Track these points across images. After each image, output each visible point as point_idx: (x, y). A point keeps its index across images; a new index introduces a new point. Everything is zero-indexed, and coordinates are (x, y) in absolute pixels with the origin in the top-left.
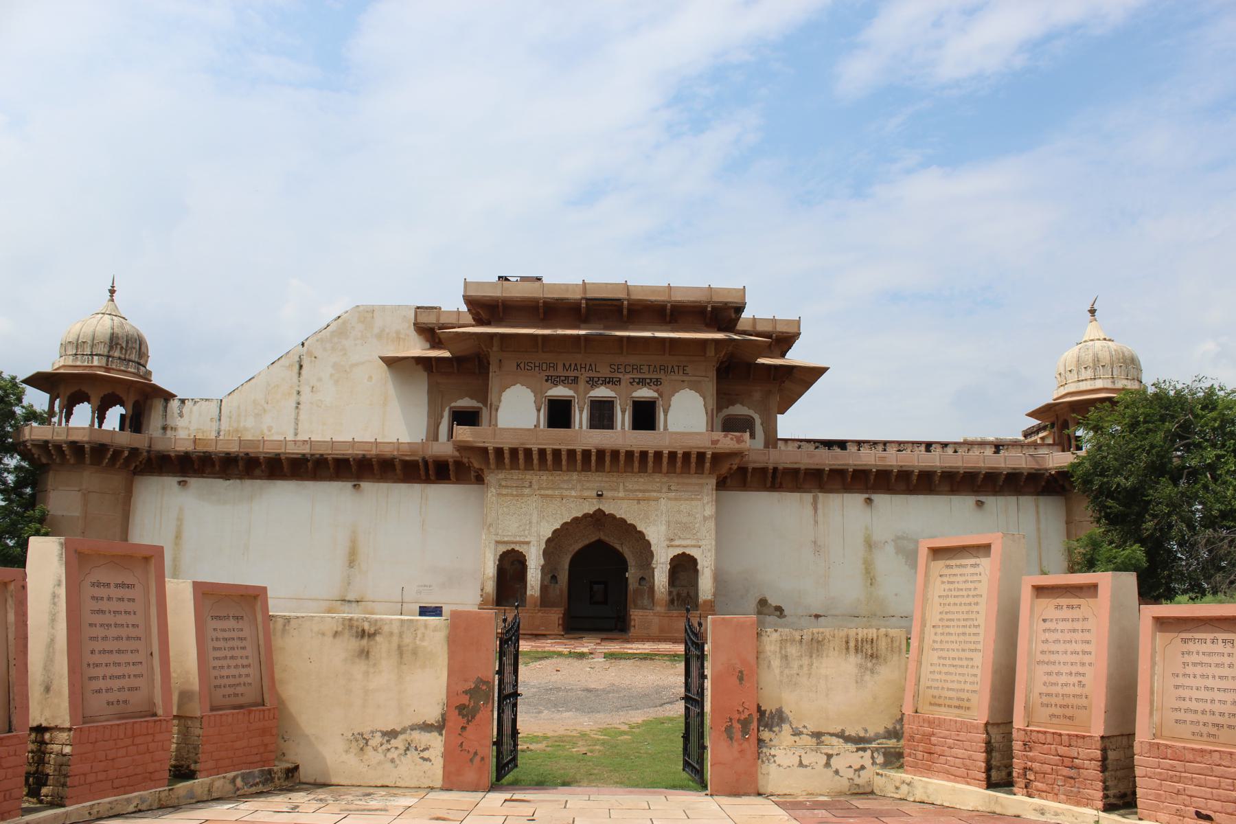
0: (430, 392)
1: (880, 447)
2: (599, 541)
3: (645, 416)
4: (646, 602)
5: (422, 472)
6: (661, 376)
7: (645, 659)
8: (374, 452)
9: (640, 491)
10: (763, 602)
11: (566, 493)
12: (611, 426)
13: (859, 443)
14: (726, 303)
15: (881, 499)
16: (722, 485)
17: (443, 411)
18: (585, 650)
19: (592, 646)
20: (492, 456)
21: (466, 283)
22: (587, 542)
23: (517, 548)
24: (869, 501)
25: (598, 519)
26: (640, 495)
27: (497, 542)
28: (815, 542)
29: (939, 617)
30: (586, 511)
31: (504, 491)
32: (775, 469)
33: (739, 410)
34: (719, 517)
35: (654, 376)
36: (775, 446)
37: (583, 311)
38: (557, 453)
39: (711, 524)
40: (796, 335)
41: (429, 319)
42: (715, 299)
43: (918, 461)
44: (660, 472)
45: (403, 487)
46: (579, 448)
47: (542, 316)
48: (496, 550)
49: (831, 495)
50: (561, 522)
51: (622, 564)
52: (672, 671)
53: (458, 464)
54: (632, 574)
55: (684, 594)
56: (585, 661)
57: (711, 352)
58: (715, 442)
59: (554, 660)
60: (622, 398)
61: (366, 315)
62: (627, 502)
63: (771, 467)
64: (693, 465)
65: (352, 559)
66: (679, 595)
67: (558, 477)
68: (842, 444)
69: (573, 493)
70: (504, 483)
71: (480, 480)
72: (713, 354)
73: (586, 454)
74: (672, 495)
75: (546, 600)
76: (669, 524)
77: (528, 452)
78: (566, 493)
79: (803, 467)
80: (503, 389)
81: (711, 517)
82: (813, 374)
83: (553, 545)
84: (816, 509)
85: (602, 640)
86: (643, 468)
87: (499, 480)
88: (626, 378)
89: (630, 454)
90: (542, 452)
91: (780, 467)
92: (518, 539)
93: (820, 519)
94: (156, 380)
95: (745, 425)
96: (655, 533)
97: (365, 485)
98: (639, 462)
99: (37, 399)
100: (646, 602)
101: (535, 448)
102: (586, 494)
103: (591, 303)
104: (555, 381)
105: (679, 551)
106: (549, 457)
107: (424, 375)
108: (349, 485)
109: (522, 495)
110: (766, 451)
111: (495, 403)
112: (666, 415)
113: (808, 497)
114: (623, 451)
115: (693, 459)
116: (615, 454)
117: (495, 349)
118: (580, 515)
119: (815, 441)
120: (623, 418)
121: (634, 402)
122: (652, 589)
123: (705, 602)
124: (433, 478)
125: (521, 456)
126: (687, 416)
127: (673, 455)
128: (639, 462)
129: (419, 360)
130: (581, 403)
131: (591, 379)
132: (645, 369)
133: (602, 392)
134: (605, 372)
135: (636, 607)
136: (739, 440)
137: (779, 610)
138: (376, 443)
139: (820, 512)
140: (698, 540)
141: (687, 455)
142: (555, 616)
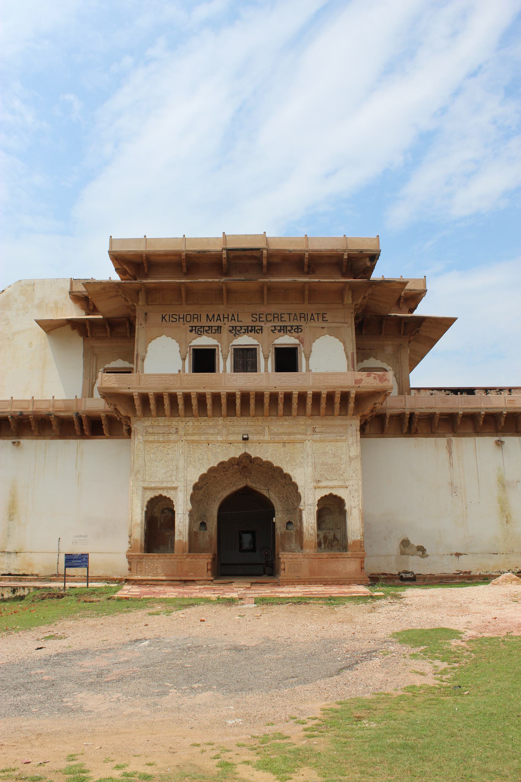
0: (85, 355)
1: (507, 392)
3: (286, 360)
4: (293, 546)
5: (77, 427)
6: (302, 323)
7: (299, 603)
8: (31, 409)
9: (285, 434)
10: (405, 543)
11: (211, 438)
13: (486, 390)
14: (361, 251)
16: (363, 431)
18: (235, 595)
19: (242, 591)
20: (137, 403)
22: (234, 489)
23: (165, 494)
24: (499, 444)
25: (245, 464)
26: (285, 438)
27: (145, 489)
28: (451, 484)
30: (232, 455)
31: (151, 438)
32: (412, 415)
33: (371, 362)
34: (364, 457)
35: (295, 323)
36: (409, 394)
37: (224, 261)
39: (357, 465)
40: (424, 292)
42: (351, 247)
44: (305, 415)
45: (60, 443)
46: (223, 391)
47: (185, 270)
48: (143, 496)
49: (464, 439)
50: (208, 467)
52: (333, 617)
53: (111, 419)
55: (331, 537)
56: (234, 608)
59: (200, 608)
60: (265, 345)
61: (27, 288)
63: (408, 412)
64: (337, 406)
65: (12, 512)
66: (325, 538)
67: (204, 423)
68: (470, 391)
69: (219, 438)
70: (150, 430)
72: (350, 301)
74: (317, 437)
75: (194, 546)
77: (173, 397)
78: (211, 438)
79: (438, 411)
81: (356, 457)
82: (443, 325)
83: (201, 490)
84: (450, 453)
85: (252, 584)
88: (267, 326)
89: (274, 397)
90: (187, 397)
91: (417, 412)
92: (165, 485)
96: (302, 475)
97: (24, 442)
100: (293, 546)
101: (179, 392)
102: (232, 438)
103: (232, 254)
104: (199, 331)
105: (326, 492)
106: (194, 402)
107: (80, 340)
108: (9, 442)
109: (169, 442)
110: (402, 397)
111: (141, 353)
113: (442, 441)
115: (337, 400)
116: (259, 396)
117: (140, 303)
118: (226, 459)
119: (445, 389)
120: (266, 363)
122: (300, 533)
123: (354, 542)
124: (87, 433)
125: (166, 401)
126: (329, 358)
127: (317, 396)
129: (73, 324)
130: (225, 351)
131: (234, 328)
132: (286, 317)
133: (245, 340)
134: (247, 321)
135: (284, 550)
136: (382, 379)
137: (421, 549)
138: (33, 401)
139: (454, 454)
140: (345, 481)
141: (331, 396)
142: (204, 561)
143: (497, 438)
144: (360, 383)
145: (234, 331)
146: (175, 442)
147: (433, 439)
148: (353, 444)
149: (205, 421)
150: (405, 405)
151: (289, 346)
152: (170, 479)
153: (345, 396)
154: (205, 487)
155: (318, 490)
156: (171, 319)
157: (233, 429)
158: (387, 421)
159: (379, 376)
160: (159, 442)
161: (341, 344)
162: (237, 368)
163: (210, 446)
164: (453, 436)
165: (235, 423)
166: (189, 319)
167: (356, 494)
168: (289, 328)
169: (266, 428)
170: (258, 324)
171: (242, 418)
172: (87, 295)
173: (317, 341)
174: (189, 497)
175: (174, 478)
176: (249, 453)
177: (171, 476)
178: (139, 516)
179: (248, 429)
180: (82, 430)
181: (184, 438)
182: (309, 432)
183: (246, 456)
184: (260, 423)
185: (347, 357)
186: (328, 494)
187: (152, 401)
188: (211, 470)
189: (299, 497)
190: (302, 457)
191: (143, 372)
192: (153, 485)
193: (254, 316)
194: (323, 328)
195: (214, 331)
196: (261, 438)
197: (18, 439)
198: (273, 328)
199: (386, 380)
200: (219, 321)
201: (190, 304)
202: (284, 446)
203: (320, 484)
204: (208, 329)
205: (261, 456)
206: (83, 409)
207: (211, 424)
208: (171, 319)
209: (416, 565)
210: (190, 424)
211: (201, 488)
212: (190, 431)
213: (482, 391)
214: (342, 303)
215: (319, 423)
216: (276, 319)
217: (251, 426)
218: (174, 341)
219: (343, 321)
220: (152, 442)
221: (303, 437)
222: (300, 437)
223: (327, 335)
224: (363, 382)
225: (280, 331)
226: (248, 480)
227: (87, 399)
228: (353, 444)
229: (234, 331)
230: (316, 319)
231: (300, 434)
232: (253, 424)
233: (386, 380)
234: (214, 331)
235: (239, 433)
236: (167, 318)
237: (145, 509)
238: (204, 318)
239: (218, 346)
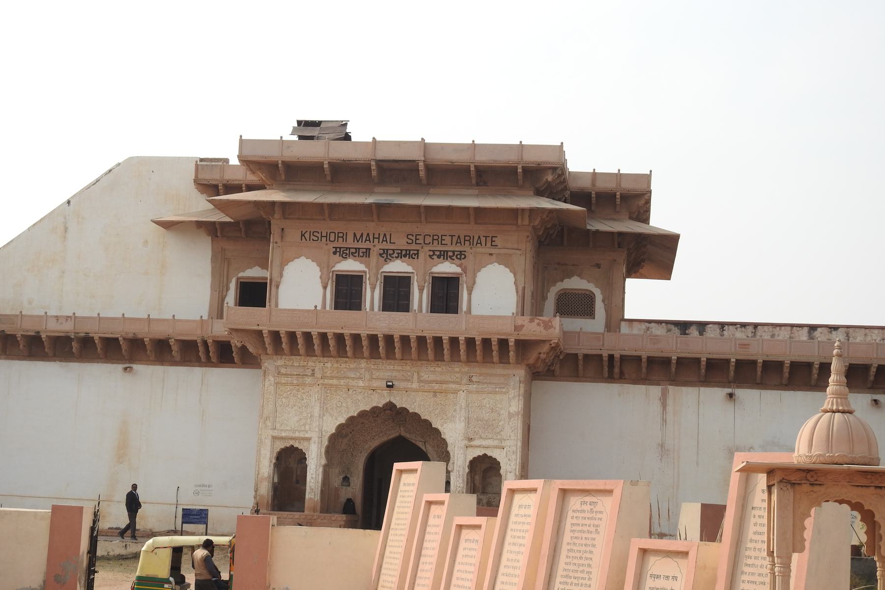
3: (446, 295)
6: (466, 248)
9: (437, 382)
11: (352, 383)
13: (722, 325)
15: (747, 395)
17: (228, 282)
21: (242, 142)
22: (385, 439)
26: (436, 386)
30: (375, 404)
31: (284, 380)
35: (458, 248)
38: (340, 338)
41: (213, 176)
49: (685, 390)
58: (518, 328)
62: (419, 392)
63: (605, 354)
69: (361, 383)
70: (283, 371)
72: (526, 222)
76: (468, 420)
77: (308, 336)
78: (352, 383)
84: (664, 405)
86: (439, 356)
87: (277, 367)
92: (297, 434)
93: (670, 417)
95: (576, 305)
102: (375, 384)
104: (344, 253)
105: (479, 452)
107: (209, 239)
108: (120, 367)
112: (470, 294)
113: (655, 391)
114: (413, 336)
117: (276, 216)
118: (368, 408)
120: (420, 297)
121: (433, 277)
126: (495, 293)
130: (373, 279)
131: (385, 251)
132: (447, 240)
133: (398, 267)
134: (401, 243)
139: (670, 408)
140: (501, 440)
143: (729, 390)
144: (520, 330)
145: (385, 255)
146: (311, 385)
147: (644, 387)
148: (514, 397)
149: (346, 362)
150: (603, 344)
151: (450, 276)
152: (303, 428)
153: (503, 343)
154: (350, 435)
155: (470, 450)
156: (312, 237)
157: (378, 374)
158: (581, 363)
159: (544, 322)
160: (292, 384)
161: (512, 275)
163: (350, 392)
164: (671, 385)
165: (380, 367)
166: (332, 239)
167: (514, 457)
168: (450, 254)
169: (415, 374)
170: (414, 247)
171: (389, 361)
173: (484, 270)
174: (323, 450)
175: (307, 427)
176: (394, 402)
177: (304, 425)
178: (266, 468)
179: (394, 374)
180: (208, 358)
181: (321, 381)
182: (464, 381)
183: (390, 406)
184: (408, 368)
185: (517, 292)
186: (481, 454)
187: (284, 340)
188: (351, 419)
190: (455, 410)
191: (277, 305)
192: (284, 434)
193: (410, 237)
194: (491, 254)
195: (361, 254)
196: (409, 385)
197: (130, 363)
198: (431, 253)
199: (551, 327)
200: (368, 242)
201: (336, 220)
202: (435, 396)
203: (472, 443)
204: (354, 251)
205: (408, 407)
206: (210, 334)
207: (352, 366)
208: (312, 237)
210: (329, 365)
211: (346, 436)
212: (328, 374)
213: (717, 326)
214: (517, 225)
215: (476, 371)
216: (436, 242)
217: (399, 371)
218: (315, 264)
219: (516, 246)
220: (285, 384)
221: (457, 386)
222: (453, 386)
223: (496, 264)
224: (525, 328)
225: (439, 257)
226: (402, 429)
227: (215, 321)
228: (514, 397)
229: (385, 255)
230: (483, 243)
231: (454, 382)
232: (400, 368)
233: (551, 327)
234: (361, 254)
235: (383, 379)
236: (307, 235)
237: (274, 461)
238: (350, 237)
239: (365, 272)
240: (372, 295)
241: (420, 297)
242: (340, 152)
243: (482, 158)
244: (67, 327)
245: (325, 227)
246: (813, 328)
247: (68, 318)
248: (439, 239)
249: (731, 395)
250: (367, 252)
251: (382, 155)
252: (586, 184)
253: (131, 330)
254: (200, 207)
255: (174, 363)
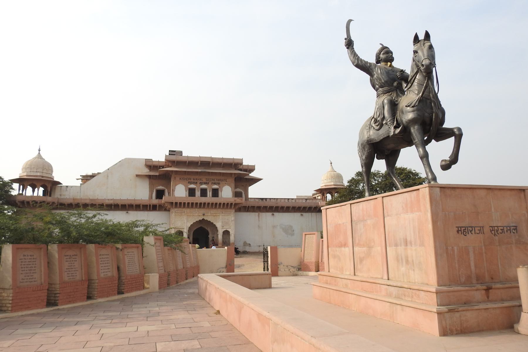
0: (149, 184)
2: (201, 227)
3: (215, 193)
12: (206, 196)
13: (270, 199)
16: (236, 211)
29: (20, 263)
38: (192, 203)
39: (233, 222)
41: (148, 163)
43: (286, 205)
51: (208, 234)
54: (210, 236)
57: (233, 176)
58: (235, 200)
62: (210, 216)
71: (169, 211)
73: (201, 204)
76: (222, 222)
79: (256, 206)
80: (176, 185)
83: (190, 229)
86: (216, 207)
94: (56, 179)
98: (215, 206)
99: (16, 186)
102: (200, 214)
104: (191, 183)
106: (190, 205)
108: (125, 212)
113: (257, 214)
114: (178, 202)
120: (209, 193)
126: (227, 192)
127: (224, 204)
128: (215, 206)
133: (204, 186)
134: (204, 181)
141: (228, 204)
162: (202, 196)
172: (151, 166)
189: (217, 231)
209: (247, 249)
215: (224, 210)
240: (198, 193)
241: (209, 193)
242: (179, 158)
243: (225, 161)
244: (111, 202)
245: (185, 177)
246: (288, 199)
247: (111, 200)
248: (214, 180)
249: (273, 214)
250: (196, 183)
251: (202, 160)
252: (246, 168)
253: (129, 203)
254: (146, 171)
255: (140, 211)
